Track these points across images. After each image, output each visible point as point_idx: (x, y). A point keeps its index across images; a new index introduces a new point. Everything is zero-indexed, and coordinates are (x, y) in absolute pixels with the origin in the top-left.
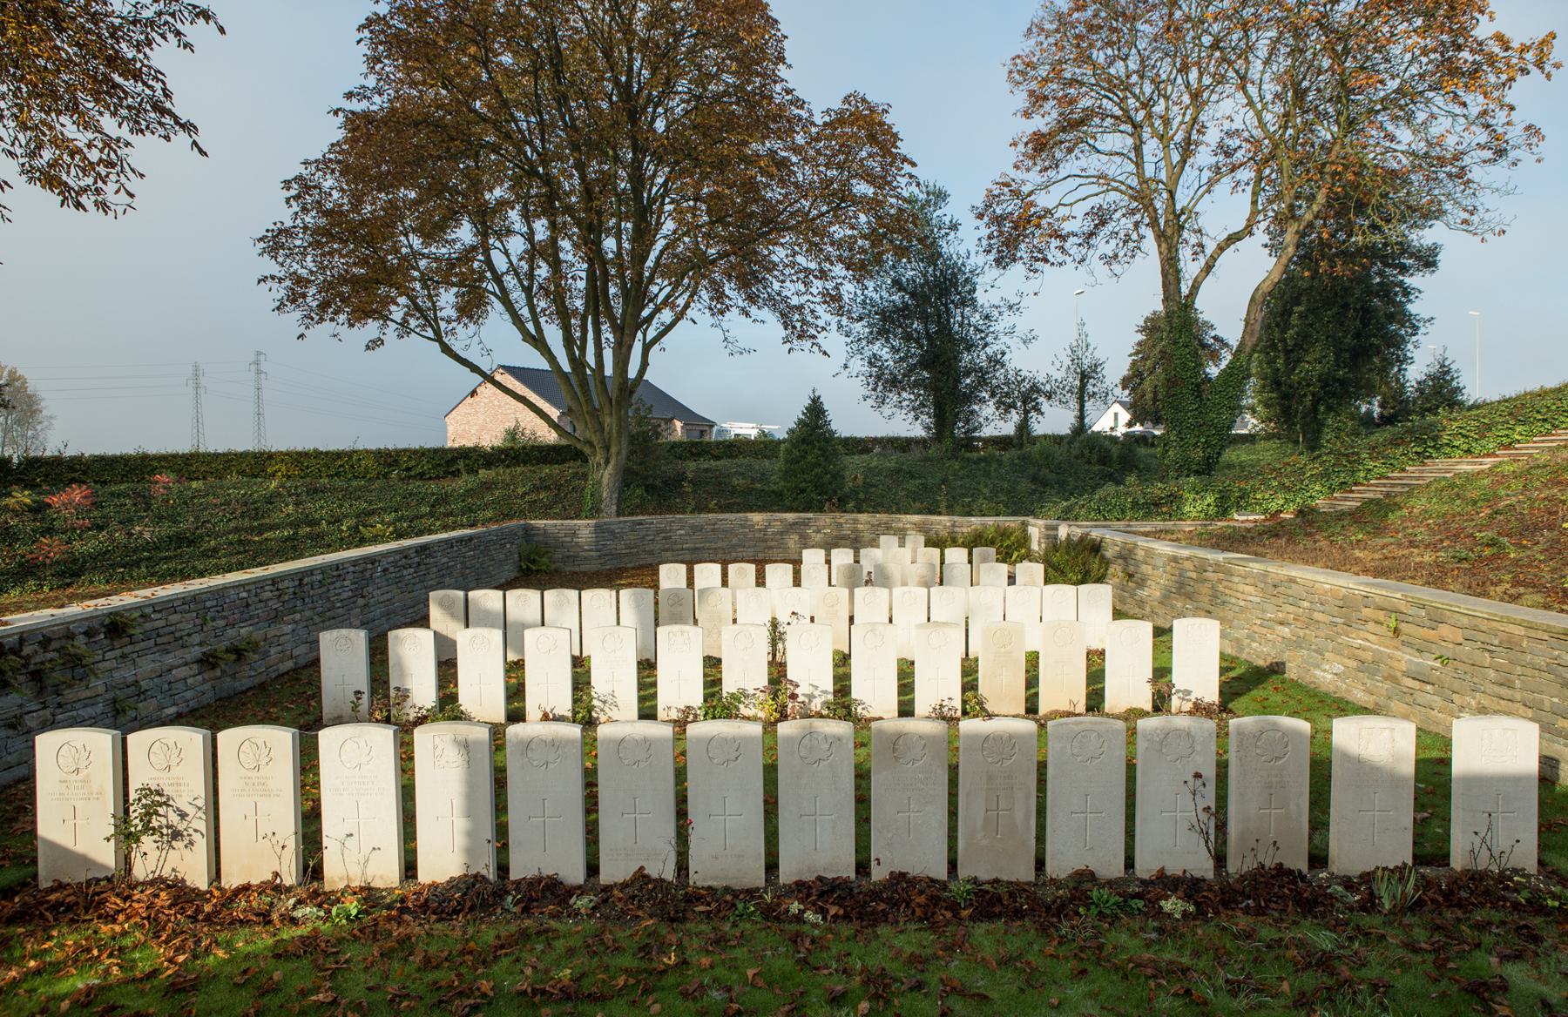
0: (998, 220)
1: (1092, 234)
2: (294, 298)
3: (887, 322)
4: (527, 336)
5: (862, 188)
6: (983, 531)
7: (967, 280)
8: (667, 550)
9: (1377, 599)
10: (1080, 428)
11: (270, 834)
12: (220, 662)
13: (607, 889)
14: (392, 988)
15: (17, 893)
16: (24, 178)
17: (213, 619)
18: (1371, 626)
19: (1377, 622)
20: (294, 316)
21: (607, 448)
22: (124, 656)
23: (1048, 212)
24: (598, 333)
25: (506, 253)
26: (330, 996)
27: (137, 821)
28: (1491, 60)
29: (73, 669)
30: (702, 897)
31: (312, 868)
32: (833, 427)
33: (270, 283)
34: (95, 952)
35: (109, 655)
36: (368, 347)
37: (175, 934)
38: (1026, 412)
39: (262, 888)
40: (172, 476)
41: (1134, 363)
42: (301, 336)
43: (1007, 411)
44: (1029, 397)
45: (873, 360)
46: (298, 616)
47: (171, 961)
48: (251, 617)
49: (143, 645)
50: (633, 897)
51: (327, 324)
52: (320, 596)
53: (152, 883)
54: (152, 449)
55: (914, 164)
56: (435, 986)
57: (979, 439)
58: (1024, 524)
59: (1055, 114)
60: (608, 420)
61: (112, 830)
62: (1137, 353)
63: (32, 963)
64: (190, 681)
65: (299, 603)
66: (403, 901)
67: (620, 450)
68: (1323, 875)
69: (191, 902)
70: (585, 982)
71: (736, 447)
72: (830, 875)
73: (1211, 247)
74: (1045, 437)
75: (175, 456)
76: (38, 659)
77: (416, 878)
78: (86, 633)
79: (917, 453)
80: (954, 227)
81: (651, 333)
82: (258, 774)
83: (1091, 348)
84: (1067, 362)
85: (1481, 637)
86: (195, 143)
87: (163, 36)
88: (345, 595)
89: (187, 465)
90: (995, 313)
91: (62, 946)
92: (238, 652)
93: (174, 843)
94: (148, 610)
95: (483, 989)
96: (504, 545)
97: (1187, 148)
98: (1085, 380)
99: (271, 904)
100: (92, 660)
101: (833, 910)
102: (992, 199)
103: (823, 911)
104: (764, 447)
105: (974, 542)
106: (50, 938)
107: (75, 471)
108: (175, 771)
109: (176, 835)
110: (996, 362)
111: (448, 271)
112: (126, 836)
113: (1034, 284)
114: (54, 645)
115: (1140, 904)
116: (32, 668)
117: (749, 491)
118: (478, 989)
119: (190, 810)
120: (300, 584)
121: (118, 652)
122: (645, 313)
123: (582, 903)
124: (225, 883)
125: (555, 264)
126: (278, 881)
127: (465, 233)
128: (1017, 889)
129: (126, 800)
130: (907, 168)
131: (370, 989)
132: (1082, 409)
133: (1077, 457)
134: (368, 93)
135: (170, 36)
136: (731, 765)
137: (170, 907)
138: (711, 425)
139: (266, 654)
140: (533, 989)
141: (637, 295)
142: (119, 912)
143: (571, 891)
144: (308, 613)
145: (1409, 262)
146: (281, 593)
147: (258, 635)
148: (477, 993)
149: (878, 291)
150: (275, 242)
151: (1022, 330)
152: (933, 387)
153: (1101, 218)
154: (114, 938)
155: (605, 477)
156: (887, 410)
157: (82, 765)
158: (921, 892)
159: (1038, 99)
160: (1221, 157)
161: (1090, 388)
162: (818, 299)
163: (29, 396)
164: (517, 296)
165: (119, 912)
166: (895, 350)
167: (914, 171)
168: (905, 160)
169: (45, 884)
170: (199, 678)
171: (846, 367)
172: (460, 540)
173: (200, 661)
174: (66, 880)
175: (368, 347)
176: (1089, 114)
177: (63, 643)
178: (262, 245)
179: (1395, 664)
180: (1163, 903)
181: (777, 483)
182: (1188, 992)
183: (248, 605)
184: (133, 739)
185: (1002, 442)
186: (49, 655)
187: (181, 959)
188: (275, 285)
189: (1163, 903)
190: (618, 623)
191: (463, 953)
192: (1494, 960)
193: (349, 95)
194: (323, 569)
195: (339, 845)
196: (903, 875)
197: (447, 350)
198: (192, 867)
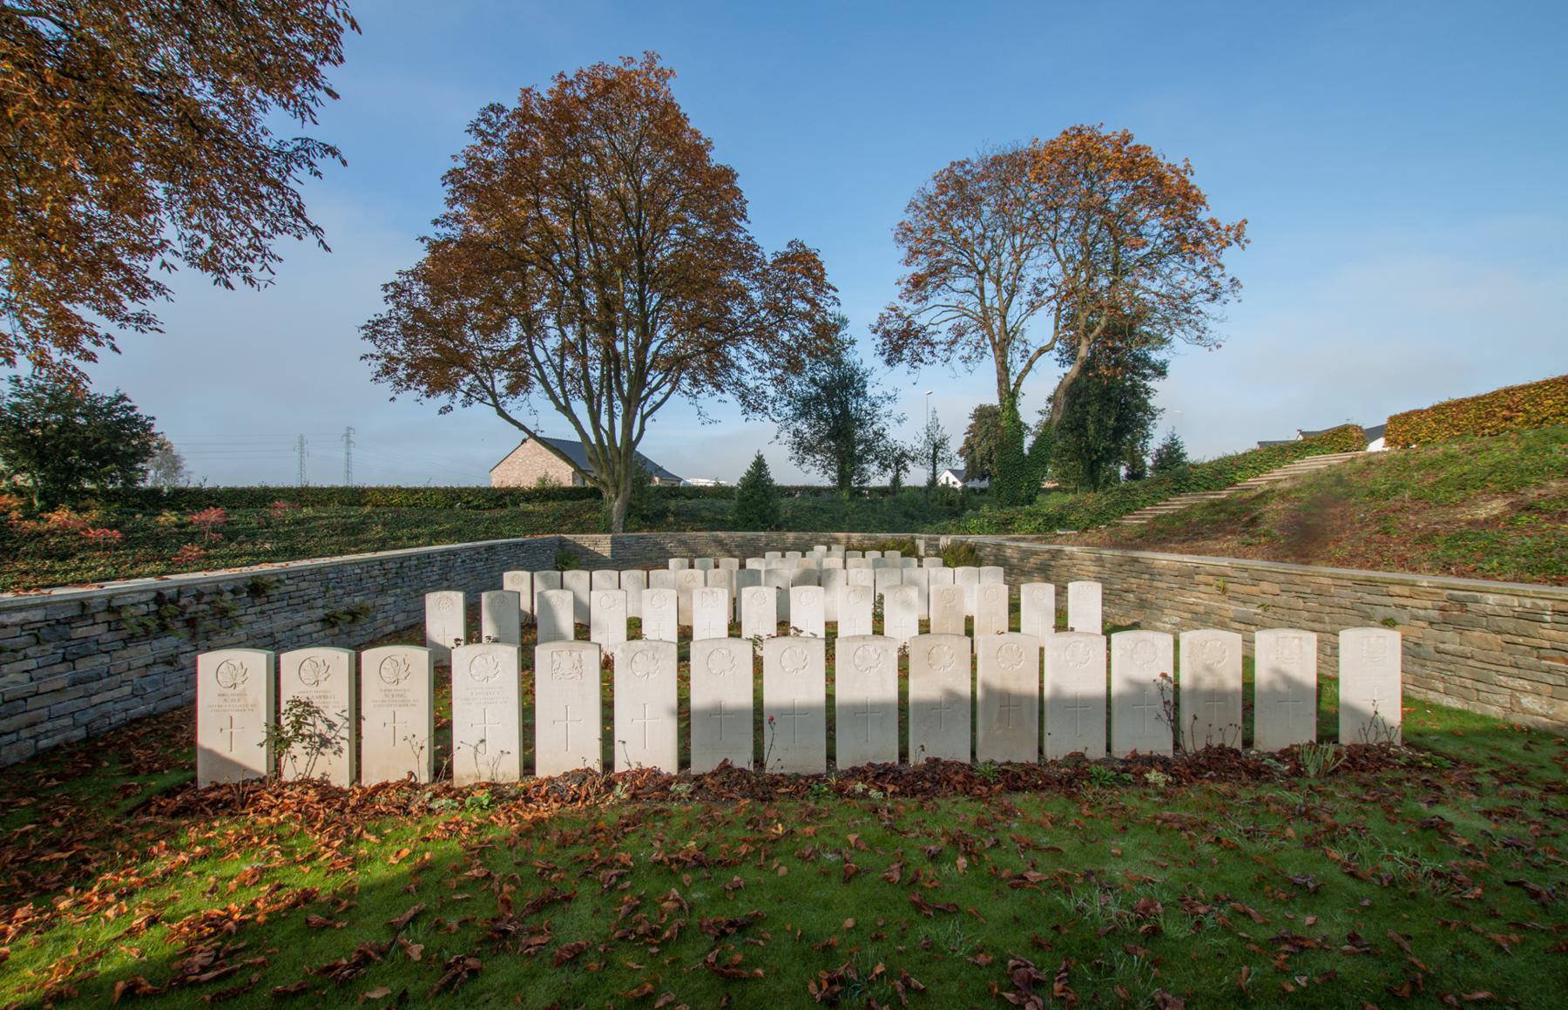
0: (887, 333)
1: (953, 342)
2: (388, 371)
3: (806, 407)
4: (560, 407)
5: (801, 306)
7: (860, 380)
9: (1208, 568)
10: (933, 482)
11: (410, 737)
12: (340, 622)
13: (697, 778)
14: (539, 863)
15: (179, 793)
16: (187, 263)
17: (334, 588)
18: (1202, 588)
19: (1206, 584)
20: (387, 385)
21: (617, 486)
22: (262, 612)
23: (924, 328)
24: (611, 407)
25: (545, 349)
26: (482, 872)
27: (289, 728)
28: (1208, 235)
29: (220, 619)
30: (778, 781)
31: (442, 766)
32: (772, 476)
33: (369, 360)
34: (256, 840)
35: (250, 611)
36: (440, 412)
37: (327, 823)
38: (898, 471)
39: (399, 786)
40: (288, 503)
41: (968, 439)
42: (393, 399)
43: (885, 470)
44: (900, 460)
45: (797, 433)
46: (398, 591)
47: (327, 845)
48: (363, 589)
49: (278, 604)
50: (723, 783)
51: (411, 392)
52: (416, 576)
53: (300, 783)
54: (273, 484)
55: (836, 290)
56: (578, 861)
57: (867, 489)
58: (913, 539)
59: (926, 264)
60: (617, 467)
61: (264, 736)
63: (198, 849)
64: (315, 635)
65: (400, 581)
66: (525, 793)
67: (626, 486)
68: (1253, 752)
69: (338, 798)
70: (710, 851)
71: (698, 492)
72: (878, 762)
73: (1033, 351)
74: (910, 487)
75: (290, 489)
76: (191, 610)
77: (534, 774)
78: (232, 591)
79: (826, 496)
80: (852, 342)
81: (647, 409)
82: (399, 687)
84: (925, 437)
85: (1296, 588)
86: (321, 241)
87: (300, 165)
88: (434, 578)
89: (300, 496)
90: (879, 402)
91: (223, 835)
92: (354, 615)
93: (322, 750)
94: (283, 577)
95: (622, 860)
96: (545, 551)
97: (1012, 293)
98: (937, 447)
99: (409, 799)
100: (237, 613)
101: (891, 788)
102: (883, 319)
103: (881, 789)
104: (720, 492)
105: (883, 548)
106: (212, 828)
107: (211, 498)
108: (323, 686)
109: (325, 742)
110: (879, 435)
111: (501, 360)
112: (278, 742)
113: (913, 377)
114: (206, 599)
115: (1130, 777)
116: (187, 616)
117: (713, 520)
118: (618, 861)
119: (339, 721)
120: (401, 567)
121: (258, 609)
122: (644, 394)
123: (683, 789)
124: (364, 783)
125: (583, 358)
126: (413, 780)
127: (515, 329)
128: (1029, 769)
129: (278, 711)
130: (831, 293)
131: (518, 864)
132: (934, 469)
134: (450, 222)
135: (305, 166)
136: (800, 672)
137: (318, 802)
138: (680, 480)
139: (374, 619)
140: (670, 860)
141: (639, 380)
142: (272, 807)
143: (669, 781)
144: (406, 589)
145: (1148, 372)
146: (386, 572)
147: (369, 603)
148: (617, 864)
149: (799, 385)
150: (374, 330)
151: (896, 413)
153: (960, 332)
154: (272, 828)
155: (616, 506)
156: (806, 467)
157: (239, 681)
158: (957, 773)
159: (914, 253)
160: (1034, 297)
161: (940, 455)
162: (768, 383)
163: (175, 457)
164: (553, 378)
165: (272, 807)
166: (810, 426)
167: (836, 295)
168: (830, 287)
169: (203, 784)
170: (322, 633)
171: (777, 437)
172: (516, 544)
173: (323, 620)
174: (221, 782)
175: (440, 412)
176: (950, 263)
177: (214, 597)
178: (364, 331)
179: (1224, 613)
180: (1147, 775)
182: (1218, 840)
183: (361, 580)
184: (285, 658)
185: (883, 491)
186: (202, 607)
187: (337, 843)
188: (374, 362)
189: (1147, 775)
191: (594, 831)
192: (1424, 806)
193: (436, 222)
194: (418, 557)
195: (472, 750)
196: (937, 760)
197: (502, 413)
198: (337, 770)
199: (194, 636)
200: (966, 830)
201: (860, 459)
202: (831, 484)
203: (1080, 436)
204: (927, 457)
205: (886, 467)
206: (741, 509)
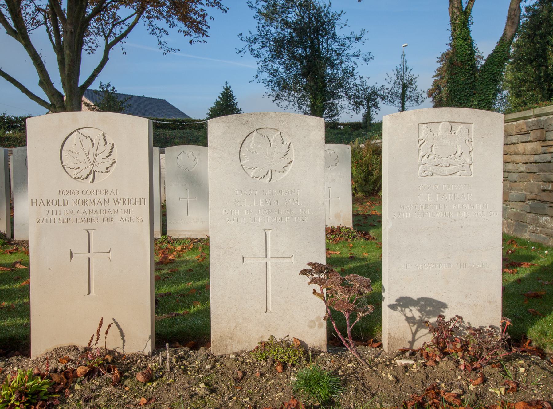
4: (10, 31)
38: (369, 108)
41: (436, 81)
45: (273, 73)
62: (437, 76)
84: (394, 78)
151: (364, 53)
199: (530, 232)
201: (333, 95)
203: (540, 66)
205: (358, 105)
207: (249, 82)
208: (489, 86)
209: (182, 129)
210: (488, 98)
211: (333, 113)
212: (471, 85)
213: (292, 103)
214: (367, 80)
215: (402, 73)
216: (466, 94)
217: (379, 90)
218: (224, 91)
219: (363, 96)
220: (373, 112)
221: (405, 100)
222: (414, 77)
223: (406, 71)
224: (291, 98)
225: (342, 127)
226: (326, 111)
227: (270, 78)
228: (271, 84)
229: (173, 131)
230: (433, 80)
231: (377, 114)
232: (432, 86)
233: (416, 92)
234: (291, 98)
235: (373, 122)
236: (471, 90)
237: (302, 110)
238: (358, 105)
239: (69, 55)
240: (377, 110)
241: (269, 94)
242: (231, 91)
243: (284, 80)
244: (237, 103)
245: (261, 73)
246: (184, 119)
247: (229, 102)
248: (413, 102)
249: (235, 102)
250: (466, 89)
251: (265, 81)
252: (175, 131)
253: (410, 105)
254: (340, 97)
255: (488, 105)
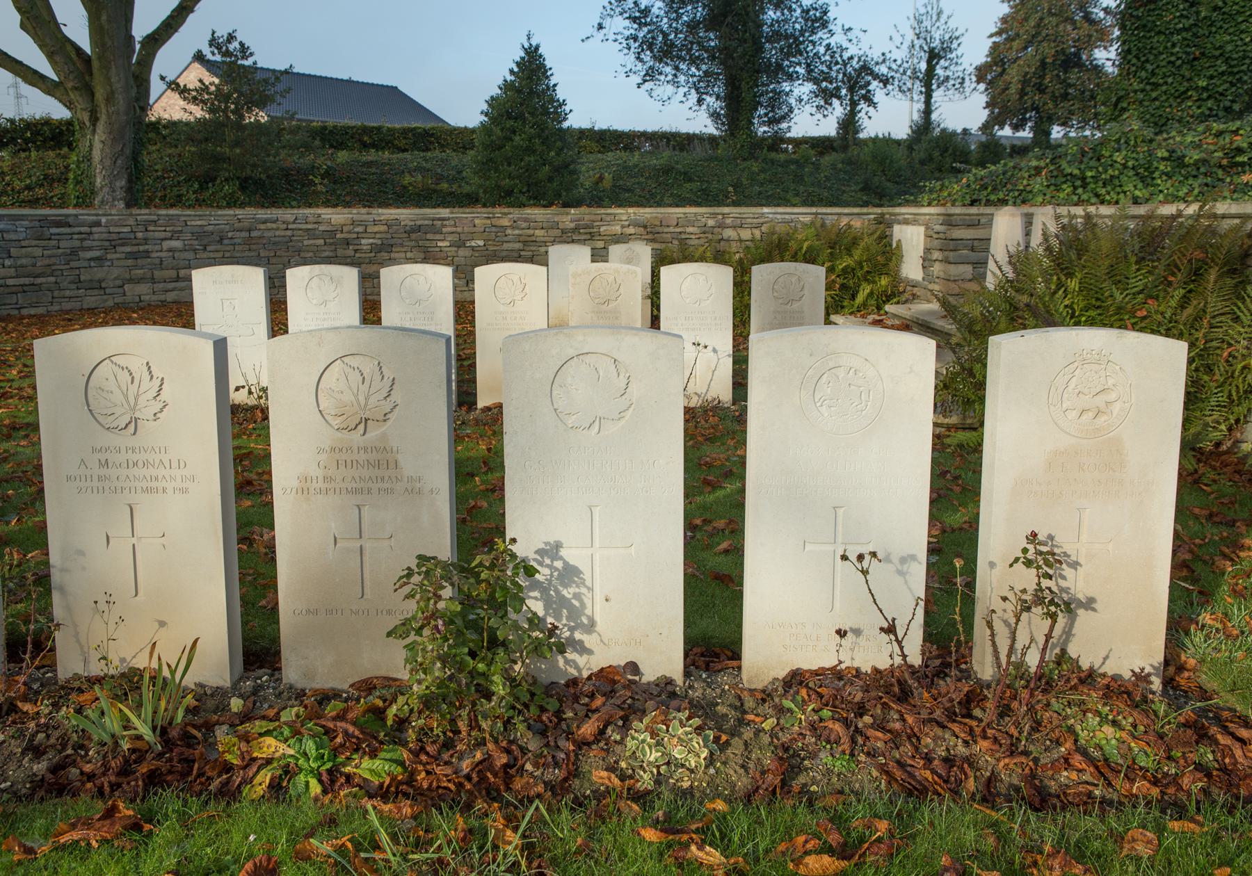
6: (789, 237)
8: (140, 280)
38: (854, 104)
41: (995, 47)
42: (681, 102)
58: (884, 224)
62: (999, 33)
79: (699, 151)
83: (944, 18)
84: (910, 36)
133: (922, 163)
152: (723, 56)
161: (939, 71)
181: (473, 183)
185: (821, 145)
190: (655, 322)
200: (125, 780)
201: (778, 71)
202: (711, 129)
204: (914, 77)
205: (828, 96)
206: (487, 166)
207: (583, 41)
208: (1243, 36)
209: (424, 151)
210: (1235, 70)
211: (780, 113)
212: (1188, 35)
213: (682, 90)
214: (861, 35)
215: (927, 23)
216: (1173, 59)
217: (877, 63)
218: (523, 55)
219: (840, 76)
220: (862, 114)
221: (934, 87)
222: (957, 34)
223: (938, 19)
224: (682, 78)
225: (790, 147)
226: (762, 111)
227: (633, 31)
228: (634, 45)
229: (401, 155)
230: (989, 43)
231: (870, 118)
232: (987, 56)
233: (961, 68)
234: (682, 78)
235: (862, 136)
236: (1188, 50)
237: (704, 107)
238: (828, 96)
239: (773, 234)
240: (871, 109)
241: (628, 69)
242: (541, 56)
243: (665, 35)
244: (555, 85)
245: (609, 19)
246: (429, 125)
247: (537, 85)
248: (951, 92)
249: (552, 83)
250: (1174, 45)
251: (619, 37)
252: (407, 155)
253: (945, 98)
254: (791, 77)
255: (1233, 89)
